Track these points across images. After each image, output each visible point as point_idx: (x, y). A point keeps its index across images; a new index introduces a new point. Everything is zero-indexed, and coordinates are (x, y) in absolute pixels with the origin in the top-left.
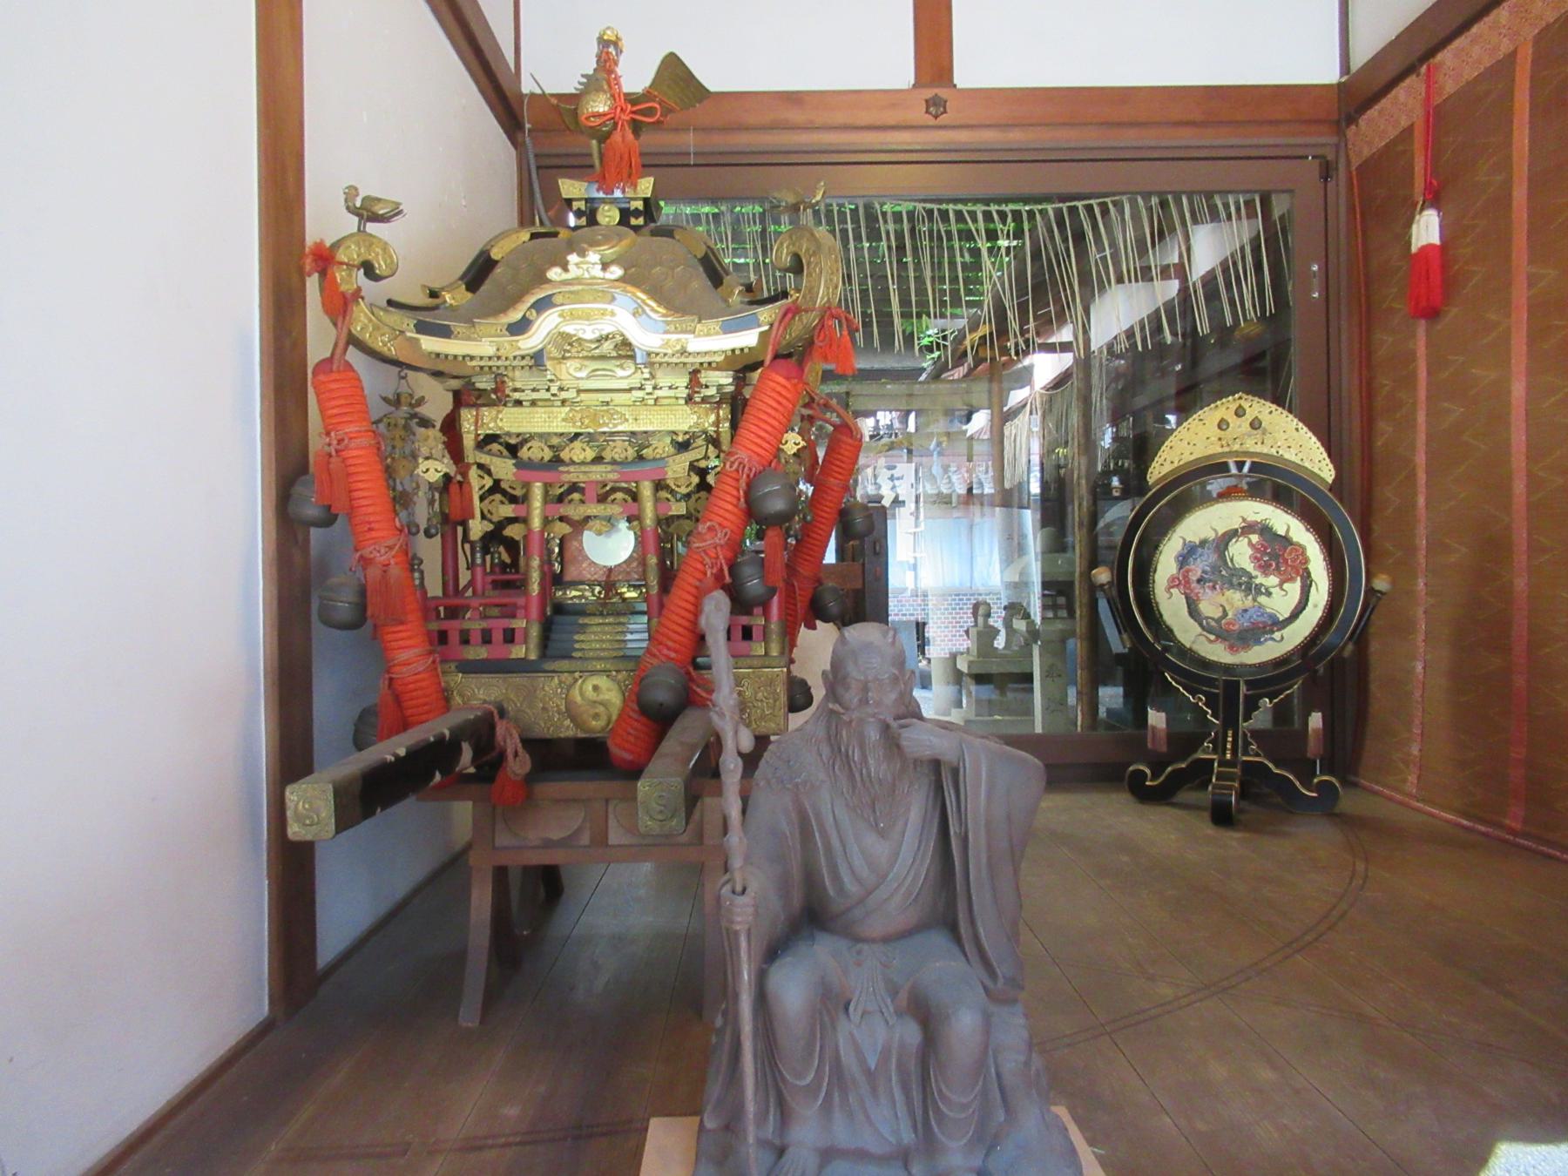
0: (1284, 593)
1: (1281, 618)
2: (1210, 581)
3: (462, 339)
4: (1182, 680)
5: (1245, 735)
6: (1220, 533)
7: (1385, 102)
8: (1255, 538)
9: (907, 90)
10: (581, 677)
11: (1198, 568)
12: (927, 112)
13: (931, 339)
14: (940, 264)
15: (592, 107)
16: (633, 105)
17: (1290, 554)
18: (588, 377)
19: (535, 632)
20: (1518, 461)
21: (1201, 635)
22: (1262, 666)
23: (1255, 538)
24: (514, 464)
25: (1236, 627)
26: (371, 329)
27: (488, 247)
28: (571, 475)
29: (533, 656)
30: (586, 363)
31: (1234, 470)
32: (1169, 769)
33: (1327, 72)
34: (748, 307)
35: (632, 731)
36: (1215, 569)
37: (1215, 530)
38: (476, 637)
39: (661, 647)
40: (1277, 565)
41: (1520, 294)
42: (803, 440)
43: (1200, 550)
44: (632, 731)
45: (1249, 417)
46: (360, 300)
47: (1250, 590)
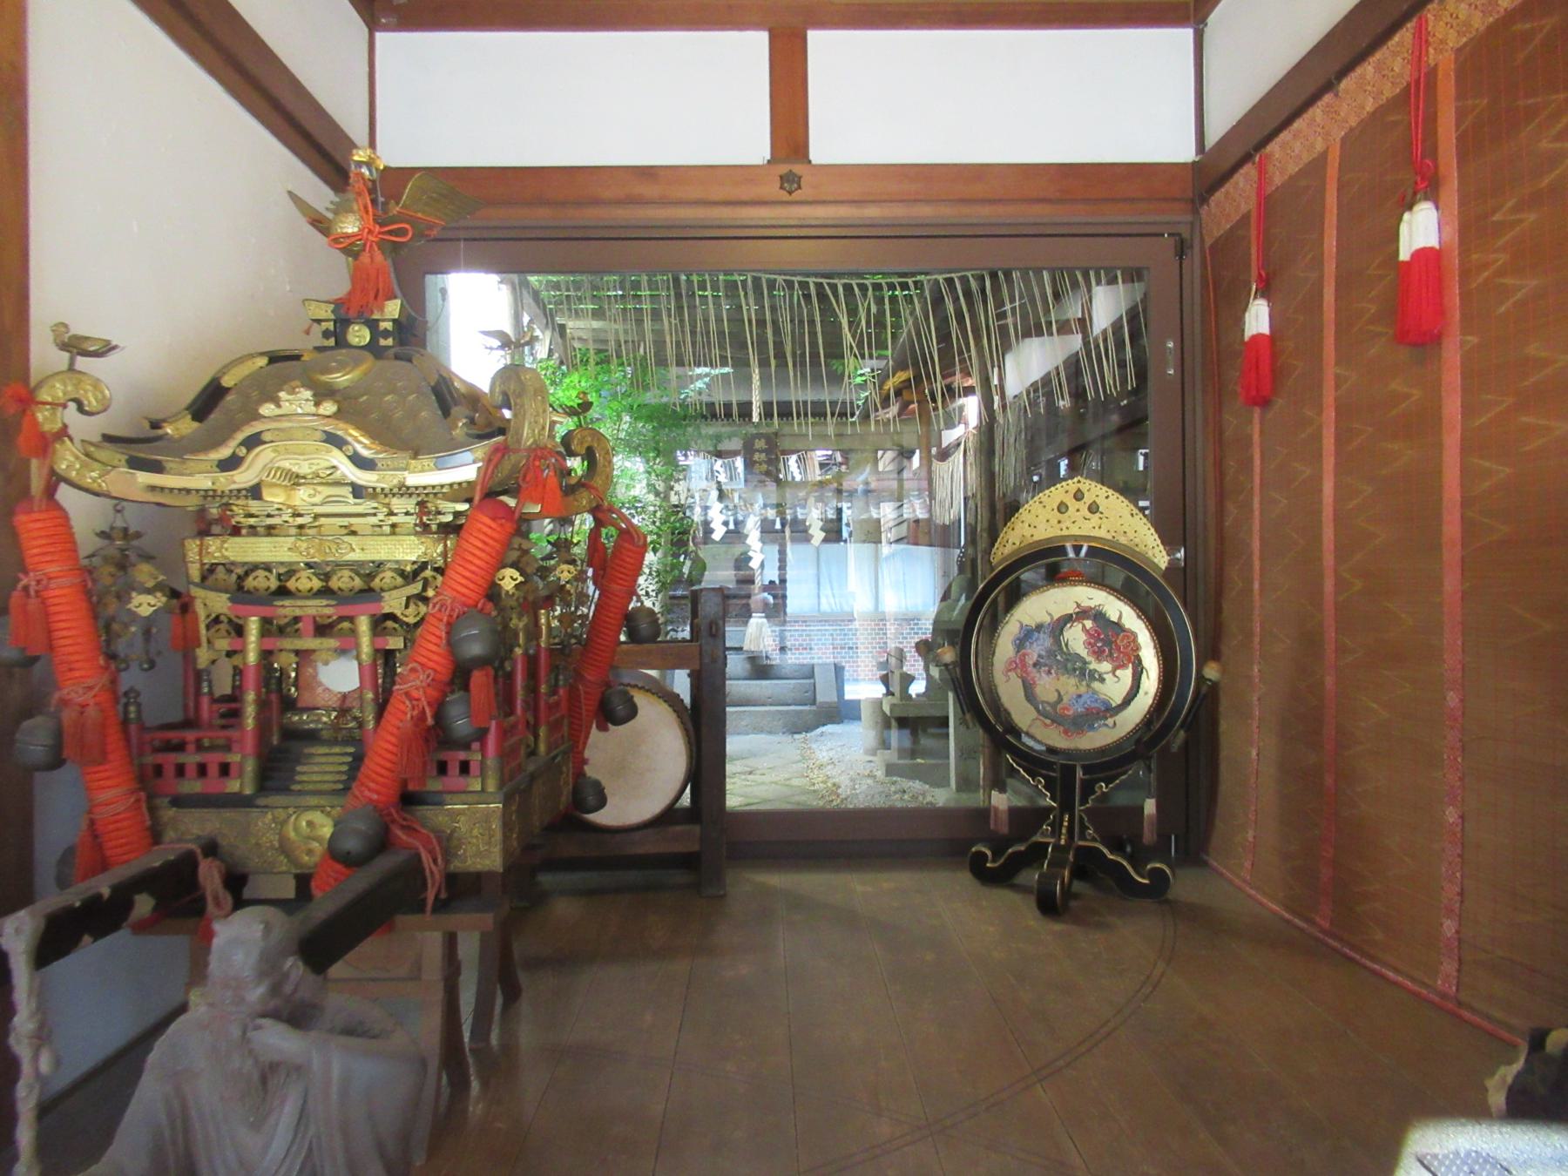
0: (1116, 679)
1: (1114, 705)
2: (1046, 665)
3: (175, 474)
4: (1024, 764)
5: (1081, 818)
6: (1056, 617)
7: (1228, 186)
8: (1089, 624)
10: (295, 812)
11: (1034, 651)
12: (782, 188)
13: (864, 378)
15: (341, 228)
16: (381, 225)
17: (1122, 641)
18: (322, 504)
19: (250, 766)
20: (1329, 559)
21: (1037, 719)
22: (1102, 751)
23: (1089, 624)
24: (229, 599)
25: (1071, 713)
26: (78, 466)
27: (219, 375)
28: (286, 609)
29: (248, 791)
30: (320, 488)
31: (1071, 555)
32: (1010, 851)
33: (1185, 152)
34: (471, 440)
35: (332, 874)
36: (1051, 654)
37: (1050, 614)
38: (191, 771)
39: (363, 788)
40: (1110, 651)
41: (1329, 396)
42: (521, 575)
44: (332, 874)
45: (1088, 499)
46: (66, 439)
47: (1084, 675)
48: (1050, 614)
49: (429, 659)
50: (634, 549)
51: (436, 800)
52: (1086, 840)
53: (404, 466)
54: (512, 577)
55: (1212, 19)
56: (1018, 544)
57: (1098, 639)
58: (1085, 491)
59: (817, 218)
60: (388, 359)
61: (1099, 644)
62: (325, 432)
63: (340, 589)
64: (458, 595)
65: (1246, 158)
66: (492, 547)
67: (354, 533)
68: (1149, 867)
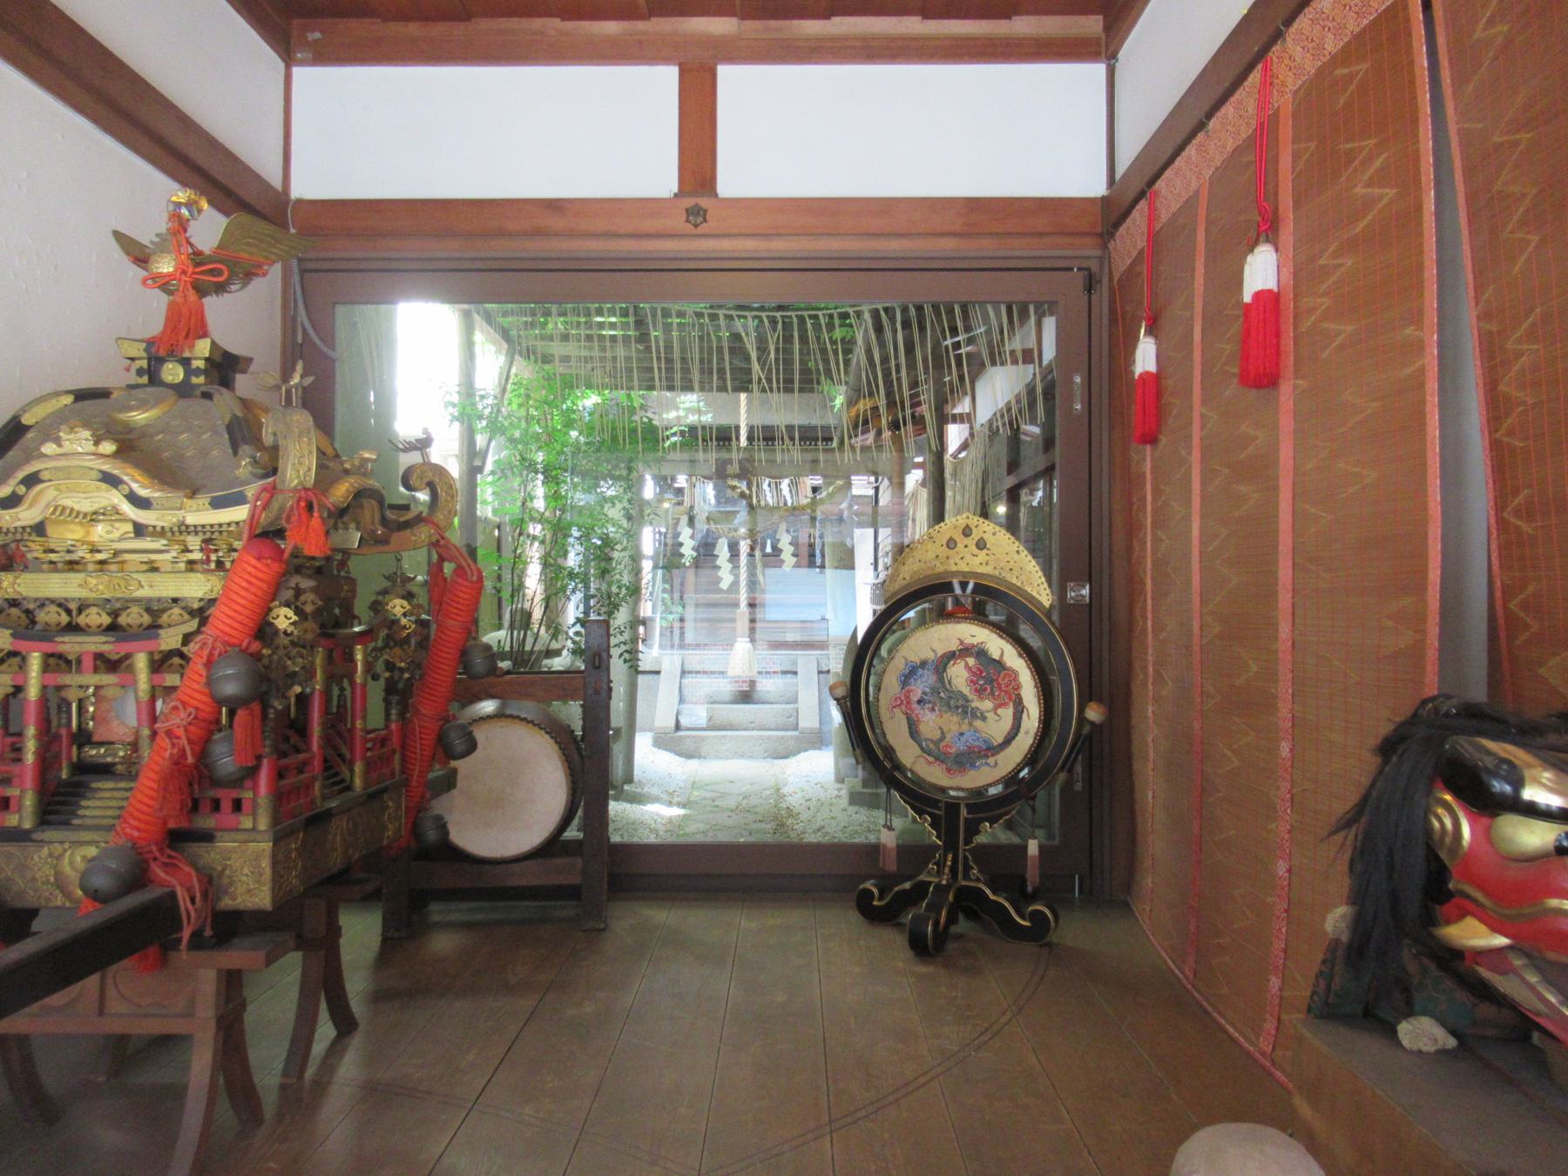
1: (995, 744)
2: (930, 702)
5: (965, 858)
6: (940, 654)
8: (971, 661)
9: (670, 199)
11: (919, 688)
12: (687, 221)
14: (710, 361)
17: (1003, 679)
19: (29, 801)
23: (971, 661)
25: (953, 750)
28: (70, 645)
29: (27, 825)
31: (958, 591)
32: (896, 889)
33: (1093, 185)
36: (935, 691)
37: (934, 651)
40: (992, 690)
42: (295, 614)
43: (920, 671)
45: (976, 535)
47: (967, 713)
48: (934, 651)
49: (192, 698)
50: (468, 584)
51: (207, 837)
52: (971, 880)
53: (178, 505)
54: (286, 616)
55: (1122, 54)
56: (908, 578)
57: (980, 676)
58: (973, 527)
59: (703, 251)
60: (196, 397)
61: (981, 682)
62: (101, 471)
63: (129, 625)
64: (221, 634)
65: (1141, 195)
66: (259, 588)
67: (155, 570)
68: (1031, 908)
